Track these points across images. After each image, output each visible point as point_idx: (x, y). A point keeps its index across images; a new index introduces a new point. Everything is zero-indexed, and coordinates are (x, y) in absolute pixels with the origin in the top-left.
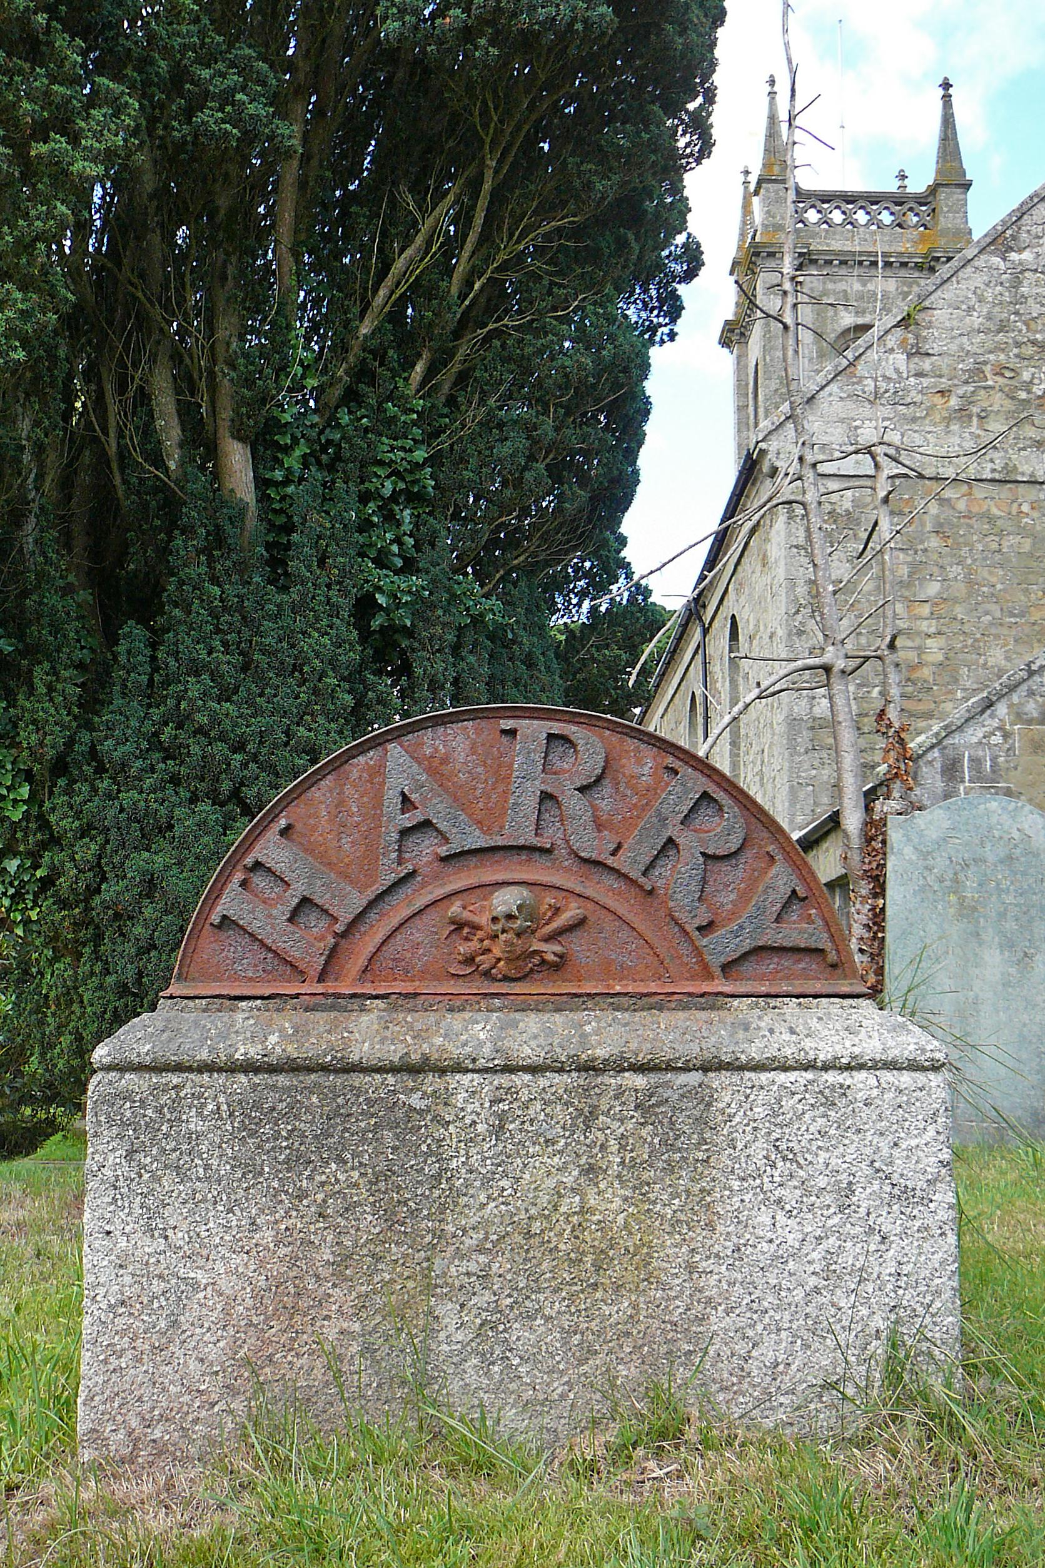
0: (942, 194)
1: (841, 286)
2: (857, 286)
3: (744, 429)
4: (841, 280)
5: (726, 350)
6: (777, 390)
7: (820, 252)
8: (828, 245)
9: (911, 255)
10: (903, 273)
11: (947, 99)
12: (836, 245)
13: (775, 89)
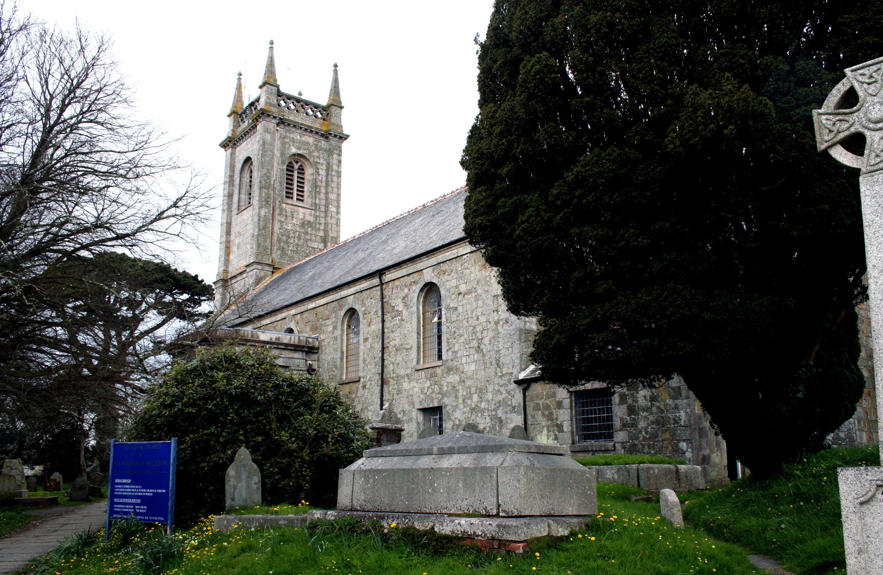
0: (333, 109)
1: (292, 136)
2: (298, 137)
9: (320, 130)
10: (316, 136)
12: (291, 118)
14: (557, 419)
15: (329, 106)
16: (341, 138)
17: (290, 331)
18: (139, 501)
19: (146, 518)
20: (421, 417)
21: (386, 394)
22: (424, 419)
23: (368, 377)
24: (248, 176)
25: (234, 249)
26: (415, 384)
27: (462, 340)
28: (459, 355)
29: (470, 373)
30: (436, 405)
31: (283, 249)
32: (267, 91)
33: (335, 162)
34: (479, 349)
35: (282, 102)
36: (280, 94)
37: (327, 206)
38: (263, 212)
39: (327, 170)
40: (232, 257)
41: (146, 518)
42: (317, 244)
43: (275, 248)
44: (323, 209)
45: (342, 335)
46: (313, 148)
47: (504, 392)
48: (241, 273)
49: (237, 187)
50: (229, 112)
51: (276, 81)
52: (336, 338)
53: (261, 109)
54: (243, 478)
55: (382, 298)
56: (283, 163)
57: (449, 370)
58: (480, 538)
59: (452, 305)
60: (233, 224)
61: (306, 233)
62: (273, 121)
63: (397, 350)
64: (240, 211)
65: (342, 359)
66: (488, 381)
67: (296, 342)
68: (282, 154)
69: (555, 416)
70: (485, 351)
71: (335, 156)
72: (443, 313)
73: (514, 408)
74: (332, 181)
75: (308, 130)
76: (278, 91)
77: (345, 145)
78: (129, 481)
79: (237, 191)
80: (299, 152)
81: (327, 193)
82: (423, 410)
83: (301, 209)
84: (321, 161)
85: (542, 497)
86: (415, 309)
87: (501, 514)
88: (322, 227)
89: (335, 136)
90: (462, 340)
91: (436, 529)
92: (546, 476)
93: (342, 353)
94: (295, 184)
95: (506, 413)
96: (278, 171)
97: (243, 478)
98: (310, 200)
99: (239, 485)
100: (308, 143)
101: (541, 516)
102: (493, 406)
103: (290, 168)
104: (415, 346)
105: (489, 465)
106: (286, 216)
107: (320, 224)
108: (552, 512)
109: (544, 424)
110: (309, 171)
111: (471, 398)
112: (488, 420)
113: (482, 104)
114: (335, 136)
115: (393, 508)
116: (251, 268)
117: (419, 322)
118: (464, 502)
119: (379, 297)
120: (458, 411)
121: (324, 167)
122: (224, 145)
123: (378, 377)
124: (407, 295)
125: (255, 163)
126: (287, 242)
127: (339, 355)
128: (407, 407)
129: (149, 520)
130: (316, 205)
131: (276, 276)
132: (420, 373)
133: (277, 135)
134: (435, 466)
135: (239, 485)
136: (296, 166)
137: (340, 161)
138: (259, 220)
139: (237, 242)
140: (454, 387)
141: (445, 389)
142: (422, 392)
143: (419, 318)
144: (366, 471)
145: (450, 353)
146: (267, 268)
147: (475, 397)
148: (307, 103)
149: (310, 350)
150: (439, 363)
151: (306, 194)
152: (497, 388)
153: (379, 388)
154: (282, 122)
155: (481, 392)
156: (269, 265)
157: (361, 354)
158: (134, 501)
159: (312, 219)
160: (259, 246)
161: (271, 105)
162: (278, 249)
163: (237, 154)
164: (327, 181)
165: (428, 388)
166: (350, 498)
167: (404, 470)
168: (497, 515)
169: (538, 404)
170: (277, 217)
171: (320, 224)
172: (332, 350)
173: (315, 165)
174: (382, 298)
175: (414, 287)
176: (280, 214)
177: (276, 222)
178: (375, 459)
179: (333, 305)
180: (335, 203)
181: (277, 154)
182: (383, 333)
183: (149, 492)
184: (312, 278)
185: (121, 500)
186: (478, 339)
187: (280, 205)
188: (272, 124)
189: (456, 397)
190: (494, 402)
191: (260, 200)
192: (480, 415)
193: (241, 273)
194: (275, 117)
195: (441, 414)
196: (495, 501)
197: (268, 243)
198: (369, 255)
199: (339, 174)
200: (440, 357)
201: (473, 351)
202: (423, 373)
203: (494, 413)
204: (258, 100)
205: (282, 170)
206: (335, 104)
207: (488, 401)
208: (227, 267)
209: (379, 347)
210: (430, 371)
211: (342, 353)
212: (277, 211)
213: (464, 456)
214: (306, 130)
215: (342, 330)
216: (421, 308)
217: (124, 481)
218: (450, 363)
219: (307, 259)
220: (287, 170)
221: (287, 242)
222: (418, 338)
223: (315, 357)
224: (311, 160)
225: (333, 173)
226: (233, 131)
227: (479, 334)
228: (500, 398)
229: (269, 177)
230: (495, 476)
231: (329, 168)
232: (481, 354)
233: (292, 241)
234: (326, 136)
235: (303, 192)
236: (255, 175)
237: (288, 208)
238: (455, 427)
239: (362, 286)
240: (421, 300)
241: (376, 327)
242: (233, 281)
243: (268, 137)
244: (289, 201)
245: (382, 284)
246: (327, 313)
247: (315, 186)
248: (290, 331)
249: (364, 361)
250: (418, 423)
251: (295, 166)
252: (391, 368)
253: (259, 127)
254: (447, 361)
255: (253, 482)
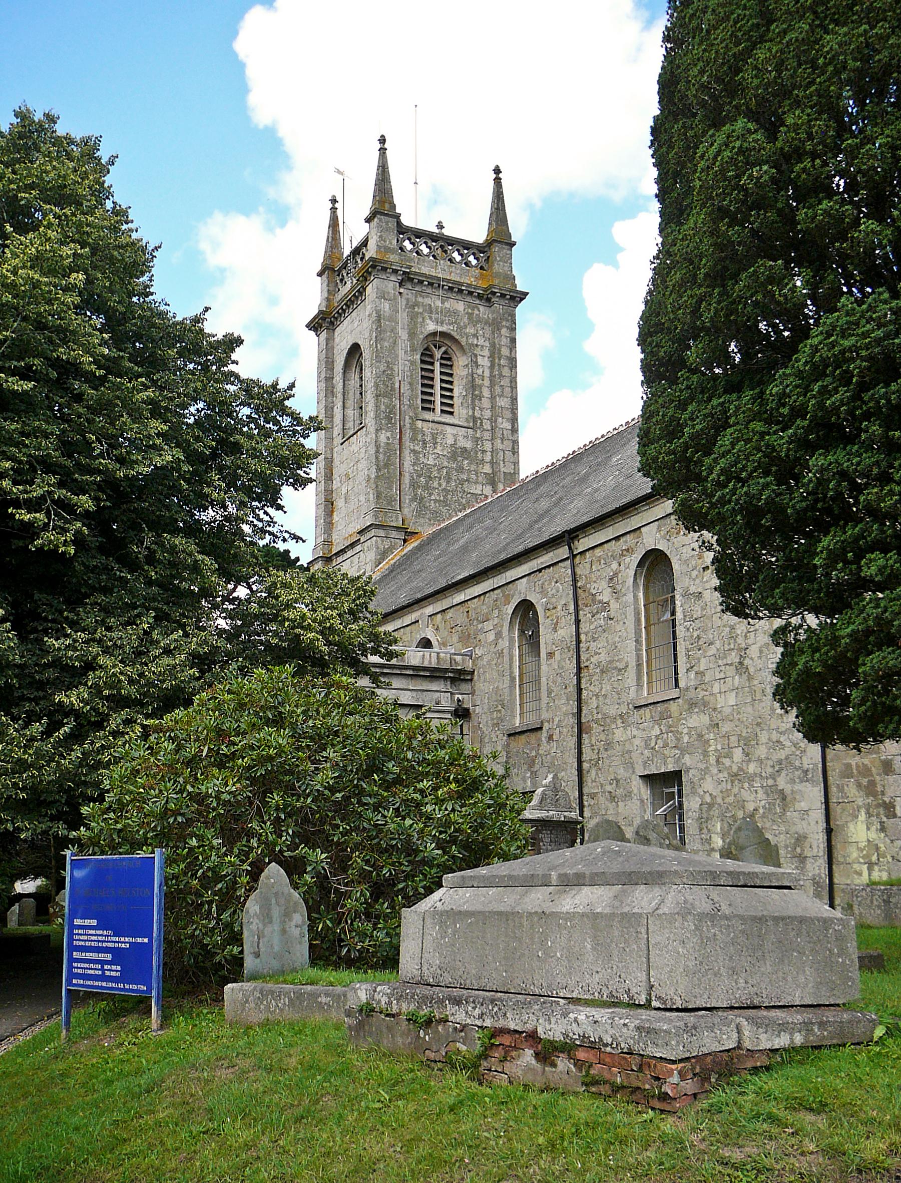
0: (496, 248)
1: (427, 301)
2: (439, 303)
3: (329, 395)
4: (427, 297)
5: (312, 333)
6: (384, 371)
7: (416, 273)
8: (419, 269)
9: (476, 287)
10: (469, 299)
11: (383, 151)
12: (425, 270)
13: (386, 146)
14: (883, 793)
15: (489, 243)
16: (512, 298)
17: (426, 644)
18: (109, 957)
19: (121, 986)
20: (645, 792)
21: (586, 750)
22: (653, 794)
23: (557, 720)
24: (357, 376)
25: (340, 503)
26: (635, 732)
27: (712, 650)
28: (707, 678)
29: (727, 711)
30: (671, 768)
31: (422, 499)
32: (379, 226)
33: (504, 341)
34: (741, 667)
35: (407, 244)
36: (402, 230)
37: (493, 420)
38: (383, 438)
39: (492, 356)
40: (336, 517)
41: (121, 986)
42: (479, 487)
43: (407, 499)
44: (487, 425)
45: (511, 648)
46: (466, 320)
47: (788, 743)
48: (352, 545)
49: (340, 396)
50: (319, 268)
51: (394, 207)
52: (501, 654)
53: (371, 259)
54: (273, 919)
55: (575, 581)
56: (413, 350)
57: (692, 704)
58: (609, 1049)
59: (692, 589)
60: (336, 462)
61: (460, 469)
62: (393, 278)
63: (602, 672)
64: (346, 439)
65: (512, 686)
66: (758, 724)
67: (434, 664)
68: (412, 335)
69: (879, 788)
70: (752, 670)
71: (504, 331)
72: (678, 603)
73: (806, 772)
74: (501, 375)
75: (455, 289)
76: (399, 223)
77: (521, 310)
78: (94, 923)
79: (339, 404)
80: (440, 329)
81: (493, 398)
82: (649, 779)
83: (449, 429)
84: (481, 342)
85: (734, 971)
86: (630, 597)
87: (654, 1004)
88: (488, 458)
89: (503, 296)
90: (712, 650)
91: (540, 1030)
92: (743, 932)
93: (513, 679)
94: (437, 384)
95: (793, 781)
96: (406, 362)
97: (273, 919)
98: (464, 412)
99: (268, 930)
100: (455, 313)
101: (732, 1008)
102: (770, 770)
103: (427, 357)
104: (633, 663)
105: (636, 910)
106: (424, 442)
107: (484, 452)
108: (756, 1002)
109: (860, 801)
110: (460, 363)
111: (729, 756)
112: (761, 794)
113: (662, 230)
114: (503, 296)
115: (483, 982)
116: (369, 535)
117: (638, 620)
118: (593, 978)
119: (569, 579)
120: (708, 779)
121: (486, 353)
122: (315, 325)
123: (573, 721)
124: (616, 574)
125: (367, 354)
126: (427, 487)
127: (507, 684)
128: (622, 773)
129: (124, 989)
130: (474, 419)
131: (410, 547)
132: (642, 711)
133: (402, 302)
134: (549, 907)
135: (268, 930)
136: (438, 354)
137: (513, 340)
138: (377, 452)
139: (344, 491)
140: (700, 736)
141: (686, 739)
142: (647, 746)
143: (637, 614)
144: (442, 913)
145: (692, 675)
146: (394, 534)
147: (738, 754)
148: (452, 242)
149: (459, 677)
150: (674, 693)
151: (457, 401)
152: (775, 736)
153: (575, 738)
154: (407, 279)
155: (748, 744)
156: (397, 528)
157: (543, 680)
158: (101, 956)
159: (469, 445)
160: (378, 496)
161: (388, 250)
162: (411, 500)
163: (337, 340)
164: (492, 376)
165: (657, 737)
166: (418, 961)
167: (500, 913)
168: (648, 1006)
169: (849, 766)
170: (407, 443)
171: (484, 452)
172: (495, 674)
173: (470, 351)
174: (575, 581)
175: (628, 560)
176: (413, 439)
177: (406, 452)
178: (461, 891)
179: (494, 595)
180: (508, 415)
181: (403, 334)
182: (578, 641)
183: (124, 942)
184: (465, 549)
185: (84, 955)
186: (740, 649)
187: (412, 424)
188: (390, 284)
189: (706, 754)
190: (770, 763)
191: (377, 417)
192: (746, 785)
193: (352, 545)
194: (395, 272)
195: (680, 784)
196: (644, 977)
197: (395, 490)
198: (556, 504)
199: (513, 363)
200: (677, 686)
201: (730, 671)
202: (647, 712)
203: (770, 782)
204: (365, 243)
205: (412, 363)
206: (500, 237)
207: (760, 761)
208: (330, 535)
209: (572, 666)
210: (659, 708)
211: (513, 679)
212: (408, 434)
213: (599, 891)
214: (451, 289)
215: (511, 640)
216: (641, 595)
217: (87, 922)
218: (692, 694)
219: (460, 515)
220: (422, 362)
221: (427, 487)
222: (638, 650)
223: (465, 687)
224: (463, 341)
225: (502, 362)
226: (328, 299)
227: (740, 640)
228: (782, 755)
229: (390, 377)
230: (643, 931)
231: (494, 353)
232: (745, 677)
233: (436, 484)
234: (486, 297)
235: (451, 398)
236: (367, 373)
237: (427, 428)
238: (705, 807)
239: (541, 560)
240: (641, 582)
241: (567, 631)
242: (340, 559)
243: (386, 306)
244: (428, 416)
245: (574, 556)
246: (485, 609)
247: (473, 386)
248: (426, 644)
249: (549, 693)
250: (642, 801)
251: (437, 351)
252: (594, 703)
253: (369, 290)
254: (687, 689)
255: (293, 923)
